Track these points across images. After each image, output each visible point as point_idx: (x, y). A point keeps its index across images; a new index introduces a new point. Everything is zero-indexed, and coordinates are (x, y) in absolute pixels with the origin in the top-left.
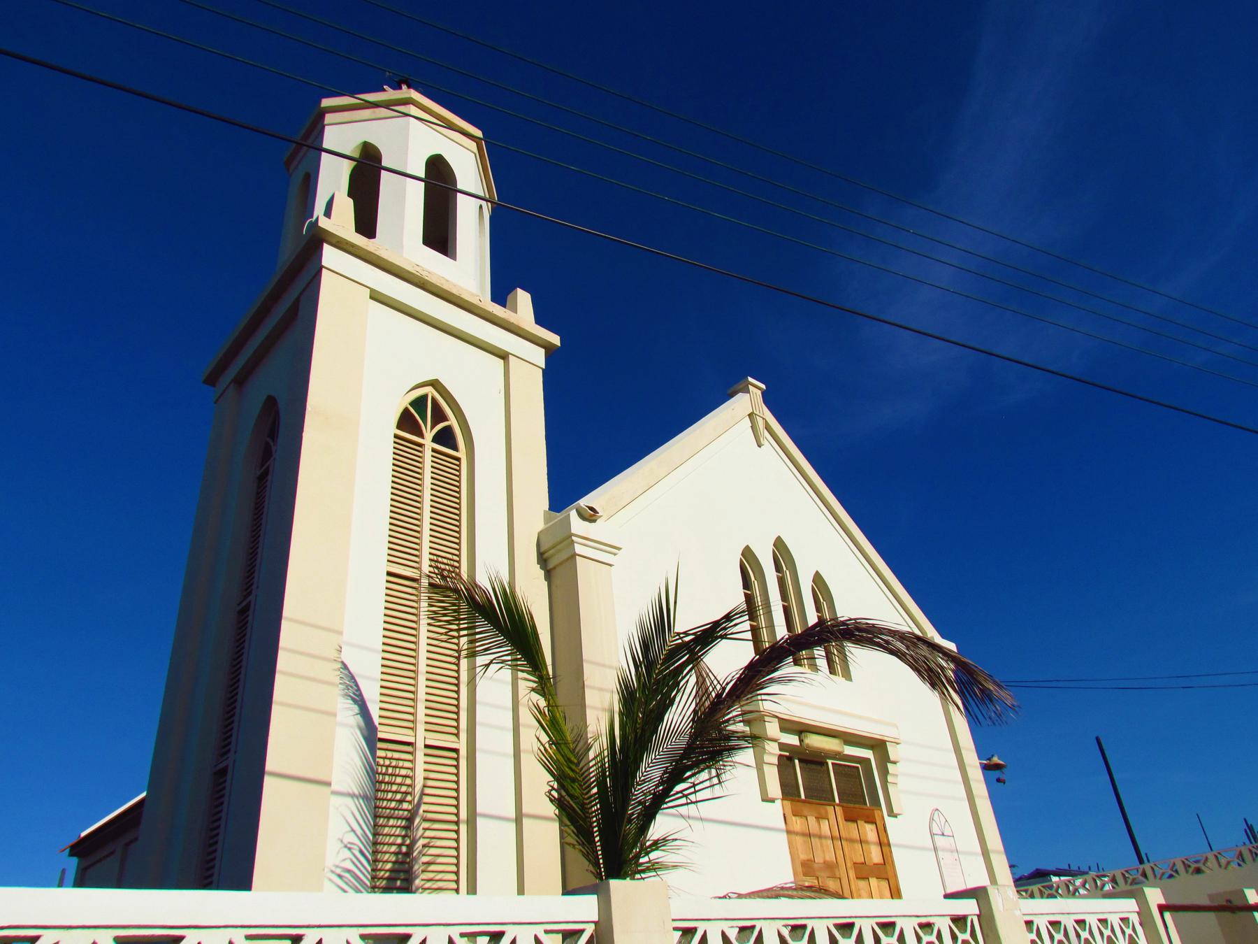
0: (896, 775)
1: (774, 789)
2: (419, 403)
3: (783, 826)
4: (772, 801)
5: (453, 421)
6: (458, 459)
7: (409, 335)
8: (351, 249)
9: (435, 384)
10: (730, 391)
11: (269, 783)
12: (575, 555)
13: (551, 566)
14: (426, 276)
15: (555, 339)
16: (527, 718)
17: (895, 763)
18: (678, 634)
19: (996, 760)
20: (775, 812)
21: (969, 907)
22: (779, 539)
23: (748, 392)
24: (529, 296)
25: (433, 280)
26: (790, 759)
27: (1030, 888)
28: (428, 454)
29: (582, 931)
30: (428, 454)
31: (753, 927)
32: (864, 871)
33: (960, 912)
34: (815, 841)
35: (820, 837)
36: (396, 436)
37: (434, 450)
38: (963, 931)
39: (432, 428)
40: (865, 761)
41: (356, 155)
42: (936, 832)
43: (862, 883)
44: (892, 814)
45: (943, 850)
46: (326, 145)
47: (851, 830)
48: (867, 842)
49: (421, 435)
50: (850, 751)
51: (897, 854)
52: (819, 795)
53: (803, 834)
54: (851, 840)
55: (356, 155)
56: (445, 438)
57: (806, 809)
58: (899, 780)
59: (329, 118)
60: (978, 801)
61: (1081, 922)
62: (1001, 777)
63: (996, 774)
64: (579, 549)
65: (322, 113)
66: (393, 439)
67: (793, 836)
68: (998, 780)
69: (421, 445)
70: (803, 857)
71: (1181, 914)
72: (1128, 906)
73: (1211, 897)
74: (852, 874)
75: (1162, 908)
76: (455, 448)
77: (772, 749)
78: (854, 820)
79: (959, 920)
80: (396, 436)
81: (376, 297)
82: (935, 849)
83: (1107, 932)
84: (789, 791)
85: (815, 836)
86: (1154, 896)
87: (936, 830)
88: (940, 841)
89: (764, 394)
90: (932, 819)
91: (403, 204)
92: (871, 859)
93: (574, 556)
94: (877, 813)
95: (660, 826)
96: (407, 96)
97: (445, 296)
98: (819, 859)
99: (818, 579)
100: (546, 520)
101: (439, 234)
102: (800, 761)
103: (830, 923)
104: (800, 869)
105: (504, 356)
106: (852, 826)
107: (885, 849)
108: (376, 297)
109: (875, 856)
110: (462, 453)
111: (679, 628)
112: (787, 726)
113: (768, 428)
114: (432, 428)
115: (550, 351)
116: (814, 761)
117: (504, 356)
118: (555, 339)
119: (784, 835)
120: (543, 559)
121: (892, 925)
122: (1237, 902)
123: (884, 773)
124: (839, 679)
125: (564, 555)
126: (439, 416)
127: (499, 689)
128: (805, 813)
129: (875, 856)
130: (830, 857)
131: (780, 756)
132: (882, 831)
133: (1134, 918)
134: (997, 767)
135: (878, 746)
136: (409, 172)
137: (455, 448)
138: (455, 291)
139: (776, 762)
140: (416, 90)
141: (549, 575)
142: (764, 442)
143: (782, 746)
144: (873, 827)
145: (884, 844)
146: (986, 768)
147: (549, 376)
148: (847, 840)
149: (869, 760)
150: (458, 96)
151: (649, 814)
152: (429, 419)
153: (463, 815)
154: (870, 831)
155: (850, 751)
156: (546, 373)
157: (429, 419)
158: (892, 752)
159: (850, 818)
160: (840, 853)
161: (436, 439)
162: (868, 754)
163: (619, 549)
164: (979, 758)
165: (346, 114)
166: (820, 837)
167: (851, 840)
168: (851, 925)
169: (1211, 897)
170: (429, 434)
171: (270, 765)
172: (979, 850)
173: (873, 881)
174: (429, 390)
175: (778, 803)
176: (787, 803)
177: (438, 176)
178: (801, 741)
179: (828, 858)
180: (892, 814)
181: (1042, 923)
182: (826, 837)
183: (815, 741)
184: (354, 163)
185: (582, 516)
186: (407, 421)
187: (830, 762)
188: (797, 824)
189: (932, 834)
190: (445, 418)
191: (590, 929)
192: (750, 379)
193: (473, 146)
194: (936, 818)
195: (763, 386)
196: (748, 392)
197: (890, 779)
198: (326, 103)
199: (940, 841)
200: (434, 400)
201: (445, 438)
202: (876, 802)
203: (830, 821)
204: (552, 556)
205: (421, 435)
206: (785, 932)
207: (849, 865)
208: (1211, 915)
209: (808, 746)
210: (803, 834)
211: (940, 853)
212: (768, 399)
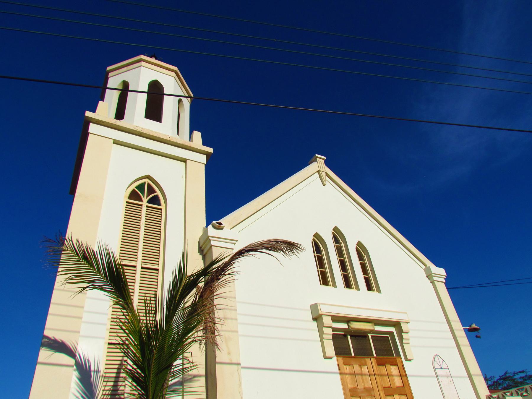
0: (408, 339)
1: (331, 350)
2: (141, 187)
3: (337, 370)
4: (331, 358)
5: (158, 193)
6: (161, 209)
7: (136, 158)
8: (103, 124)
9: (148, 177)
10: (310, 162)
12: (211, 246)
13: (205, 252)
14: (140, 130)
17: (407, 333)
18: (189, 276)
19: (474, 326)
20: (333, 363)
22: (336, 229)
23: (317, 161)
24: (200, 133)
25: (144, 132)
26: (345, 336)
27: (511, 390)
28: (144, 209)
30: (144, 209)
34: (359, 377)
35: (362, 375)
36: (127, 202)
37: (147, 207)
39: (147, 197)
40: (392, 333)
41: (121, 88)
42: (438, 365)
44: (406, 359)
45: (442, 376)
47: (383, 370)
48: (392, 375)
49: (141, 201)
50: (378, 328)
51: (412, 381)
52: (363, 352)
53: (351, 374)
54: (382, 375)
55: (121, 88)
57: (352, 361)
58: (410, 341)
60: (462, 348)
62: (479, 335)
63: (475, 333)
64: (213, 243)
66: (126, 204)
67: (344, 376)
68: (477, 336)
69: (141, 205)
70: (350, 386)
74: (382, 394)
76: (160, 205)
77: (328, 332)
78: (384, 365)
80: (127, 202)
81: (116, 142)
82: (437, 376)
84: (339, 353)
85: (358, 374)
87: (437, 366)
88: (439, 372)
91: (138, 104)
92: (394, 384)
94: (398, 360)
97: (151, 137)
98: (361, 387)
99: (359, 244)
101: (154, 111)
102: (351, 336)
104: (348, 393)
105: (184, 161)
106: (381, 367)
107: (404, 378)
108: (116, 142)
109: (398, 382)
110: (163, 207)
111: (189, 274)
112: (336, 319)
113: (328, 176)
114: (147, 197)
115: (207, 154)
116: (360, 336)
117: (184, 161)
118: (211, 150)
119: (338, 376)
120: (201, 250)
123: (401, 338)
124: (374, 294)
126: (151, 190)
129: (398, 382)
130: (368, 384)
131: (333, 334)
134: (475, 330)
135: (397, 324)
136: (139, 90)
137: (160, 205)
138: (156, 135)
139: (331, 337)
140: (144, 55)
142: (327, 183)
143: (334, 329)
144: (396, 367)
145: (403, 375)
146: (470, 331)
147: (209, 167)
148: (378, 375)
149: (392, 332)
152: (146, 194)
154: (394, 370)
155: (378, 328)
156: (207, 166)
157: (146, 194)
158: (404, 327)
160: (374, 383)
161: (149, 202)
163: (237, 241)
164: (463, 326)
166: (362, 375)
167: (382, 375)
170: (145, 200)
172: (466, 375)
174: (147, 181)
175: (335, 358)
176: (341, 359)
178: (348, 326)
179: (366, 386)
180: (406, 359)
182: (365, 375)
184: (120, 91)
185: (214, 227)
186: (134, 195)
187: (370, 335)
188: (347, 369)
189: (435, 369)
190: (154, 192)
192: (317, 155)
193: (174, 74)
194: (436, 359)
195: (325, 158)
196: (317, 161)
197: (404, 341)
198: (109, 68)
199: (439, 372)
200: (149, 184)
201: (155, 200)
202: (398, 354)
203: (370, 365)
204: (205, 248)
205: (141, 201)
207: (380, 388)
209: (352, 328)
210: (351, 374)
211: (440, 379)
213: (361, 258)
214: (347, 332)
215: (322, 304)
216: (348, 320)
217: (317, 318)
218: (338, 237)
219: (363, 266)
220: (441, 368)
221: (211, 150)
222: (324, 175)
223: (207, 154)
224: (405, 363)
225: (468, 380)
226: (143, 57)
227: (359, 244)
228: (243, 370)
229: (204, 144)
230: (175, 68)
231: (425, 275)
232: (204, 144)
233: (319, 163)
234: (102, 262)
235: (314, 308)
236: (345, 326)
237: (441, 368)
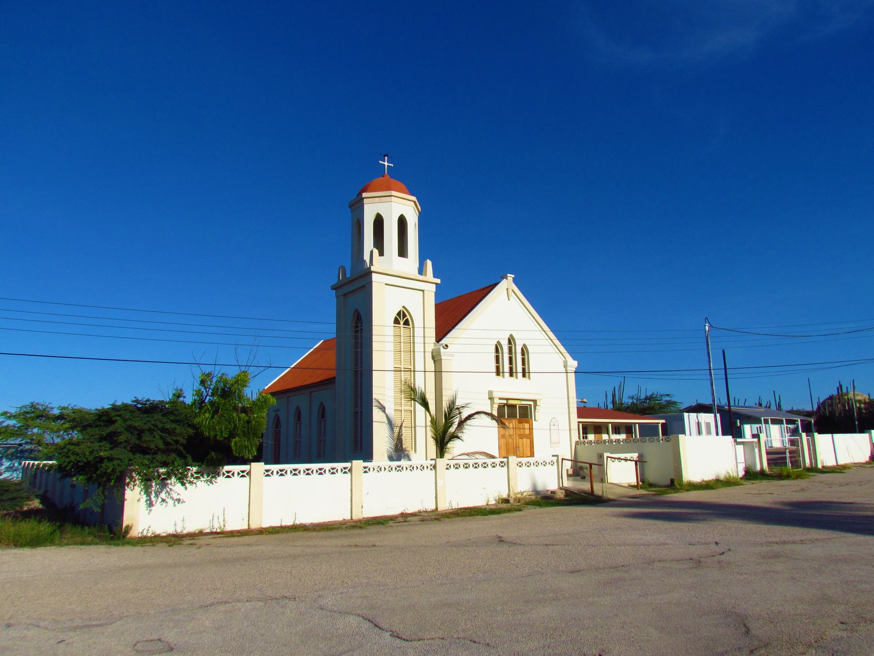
11: (374, 424)
16: (428, 428)
19: (585, 400)
46: (434, 507)
47: (521, 426)
50: (523, 402)
51: (535, 432)
52: (512, 415)
95: (449, 445)
101: (403, 251)
109: (527, 432)
120: (433, 358)
126: (404, 316)
127: (420, 409)
135: (535, 401)
141: (435, 362)
145: (531, 429)
151: (447, 443)
155: (523, 402)
157: (402, 318)
162: (532, 403)
170: (402, 323)
171: (374, 419)
177: (402, 222)
183: (511, 402)
186: (396, 321)
199: (552, 427)
212: (515, 281)
213: (523, 354)
214: (504, 405)
216: (507, 399)
217: (491, 399)
218: (511, 341)
219: (523, 360)
221: (438, 281)
222: (510, 291)
223: (436, 284)
226: (394, 193)
229: (435, 277)
230: (414, 198)
232: (435, 277)
233: (507, 284)
234: (561, 495)
235: (490, 392)
236: (505, 402)
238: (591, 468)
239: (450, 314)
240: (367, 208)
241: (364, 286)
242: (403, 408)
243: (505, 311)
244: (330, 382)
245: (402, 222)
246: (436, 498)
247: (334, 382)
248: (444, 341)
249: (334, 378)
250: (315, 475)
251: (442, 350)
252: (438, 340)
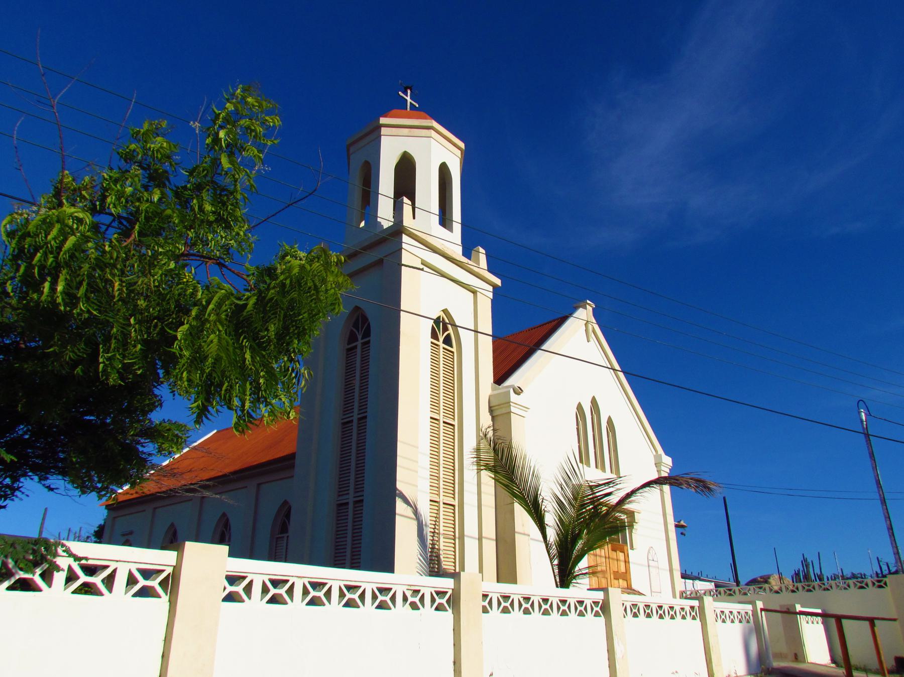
11: (397, 517)
13: (495, 414)
15: (498, 282)
19: (682, 523)
21: (695, 603)
29: (163, 571)
31: (391, 589)
32: (617, 576)
33: (692, 605)
38: (581, 611)
43: (616, 582)
44: (632, 548)
47: (613, 555)
56: (447, 341)
59: (384, 131)
61: (722, 612)
64: (513, 409)
65: (380, 127)
71: (768, 613)
72: (749, 607)
73: (781, 606)
75: (762, 610)
76: (452, 347)
79: (692, 608)
83: (723, 617)
86: (760, 605)
87: (650, 558)
89: (593, 309)
90: (649, 552)
93: (510, 412)
96: (430, 125)
99: (610, 418)
100: (493, 389)
103: (433, 590)
105: (474, 292)
106: (614, 553)
109: (623, 569)
115: (495, 287)
120: (491, 410)
121: (565, 601)
122: (791, 610)
125: (504, 411)
128: (201, 396)
132: (627, 556)
133: (750, 613)
134: (683, 526)
137: (452, 347)
145: (627, 562)
146: (676, 526)
150: (454, 124)
153: (457, 535)
154: (621, 556)
156: (492, 301)
159: (614, 550)
165: (394, 129)
166: (601, 556)
168: (509, 597)
169: (781, 606)
170: (441, 339)
171: (397, 511)
173: (621, 581)
177: (444, 171)
181: (628, 605)
191: (450, 592)
198: (383, 121)
201: (447, 341)
202: (625, 542)
206: (521, 600)
208: (779, 615)
215: (878, 619)
220: (872, 621)
223: (495, 287)
224: (630, 551)
225: (668, 573)
227: (610, 418)
228: (532, 542)
230: (462, 145)
231: (653, 462)
237: (872, 621)
238: (872, 625)
239: (515, 347)
240: (384, 141)
241: (380, 262)
242: (442, 499)
243: (577, 365)
244: (286, 463)
245: (444, 171)
246: (165, 656)
247: (292, 466)
248: (514, 380)
249: (292, 457)
250: (335, 606)
251: (513, 397)
252: (500, 377)
